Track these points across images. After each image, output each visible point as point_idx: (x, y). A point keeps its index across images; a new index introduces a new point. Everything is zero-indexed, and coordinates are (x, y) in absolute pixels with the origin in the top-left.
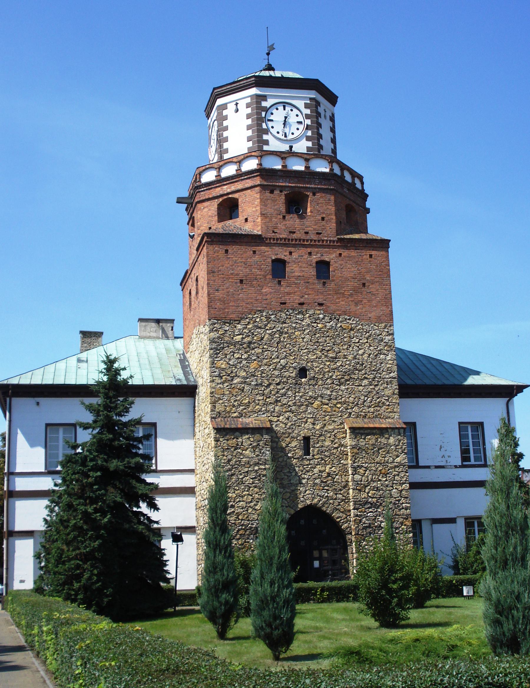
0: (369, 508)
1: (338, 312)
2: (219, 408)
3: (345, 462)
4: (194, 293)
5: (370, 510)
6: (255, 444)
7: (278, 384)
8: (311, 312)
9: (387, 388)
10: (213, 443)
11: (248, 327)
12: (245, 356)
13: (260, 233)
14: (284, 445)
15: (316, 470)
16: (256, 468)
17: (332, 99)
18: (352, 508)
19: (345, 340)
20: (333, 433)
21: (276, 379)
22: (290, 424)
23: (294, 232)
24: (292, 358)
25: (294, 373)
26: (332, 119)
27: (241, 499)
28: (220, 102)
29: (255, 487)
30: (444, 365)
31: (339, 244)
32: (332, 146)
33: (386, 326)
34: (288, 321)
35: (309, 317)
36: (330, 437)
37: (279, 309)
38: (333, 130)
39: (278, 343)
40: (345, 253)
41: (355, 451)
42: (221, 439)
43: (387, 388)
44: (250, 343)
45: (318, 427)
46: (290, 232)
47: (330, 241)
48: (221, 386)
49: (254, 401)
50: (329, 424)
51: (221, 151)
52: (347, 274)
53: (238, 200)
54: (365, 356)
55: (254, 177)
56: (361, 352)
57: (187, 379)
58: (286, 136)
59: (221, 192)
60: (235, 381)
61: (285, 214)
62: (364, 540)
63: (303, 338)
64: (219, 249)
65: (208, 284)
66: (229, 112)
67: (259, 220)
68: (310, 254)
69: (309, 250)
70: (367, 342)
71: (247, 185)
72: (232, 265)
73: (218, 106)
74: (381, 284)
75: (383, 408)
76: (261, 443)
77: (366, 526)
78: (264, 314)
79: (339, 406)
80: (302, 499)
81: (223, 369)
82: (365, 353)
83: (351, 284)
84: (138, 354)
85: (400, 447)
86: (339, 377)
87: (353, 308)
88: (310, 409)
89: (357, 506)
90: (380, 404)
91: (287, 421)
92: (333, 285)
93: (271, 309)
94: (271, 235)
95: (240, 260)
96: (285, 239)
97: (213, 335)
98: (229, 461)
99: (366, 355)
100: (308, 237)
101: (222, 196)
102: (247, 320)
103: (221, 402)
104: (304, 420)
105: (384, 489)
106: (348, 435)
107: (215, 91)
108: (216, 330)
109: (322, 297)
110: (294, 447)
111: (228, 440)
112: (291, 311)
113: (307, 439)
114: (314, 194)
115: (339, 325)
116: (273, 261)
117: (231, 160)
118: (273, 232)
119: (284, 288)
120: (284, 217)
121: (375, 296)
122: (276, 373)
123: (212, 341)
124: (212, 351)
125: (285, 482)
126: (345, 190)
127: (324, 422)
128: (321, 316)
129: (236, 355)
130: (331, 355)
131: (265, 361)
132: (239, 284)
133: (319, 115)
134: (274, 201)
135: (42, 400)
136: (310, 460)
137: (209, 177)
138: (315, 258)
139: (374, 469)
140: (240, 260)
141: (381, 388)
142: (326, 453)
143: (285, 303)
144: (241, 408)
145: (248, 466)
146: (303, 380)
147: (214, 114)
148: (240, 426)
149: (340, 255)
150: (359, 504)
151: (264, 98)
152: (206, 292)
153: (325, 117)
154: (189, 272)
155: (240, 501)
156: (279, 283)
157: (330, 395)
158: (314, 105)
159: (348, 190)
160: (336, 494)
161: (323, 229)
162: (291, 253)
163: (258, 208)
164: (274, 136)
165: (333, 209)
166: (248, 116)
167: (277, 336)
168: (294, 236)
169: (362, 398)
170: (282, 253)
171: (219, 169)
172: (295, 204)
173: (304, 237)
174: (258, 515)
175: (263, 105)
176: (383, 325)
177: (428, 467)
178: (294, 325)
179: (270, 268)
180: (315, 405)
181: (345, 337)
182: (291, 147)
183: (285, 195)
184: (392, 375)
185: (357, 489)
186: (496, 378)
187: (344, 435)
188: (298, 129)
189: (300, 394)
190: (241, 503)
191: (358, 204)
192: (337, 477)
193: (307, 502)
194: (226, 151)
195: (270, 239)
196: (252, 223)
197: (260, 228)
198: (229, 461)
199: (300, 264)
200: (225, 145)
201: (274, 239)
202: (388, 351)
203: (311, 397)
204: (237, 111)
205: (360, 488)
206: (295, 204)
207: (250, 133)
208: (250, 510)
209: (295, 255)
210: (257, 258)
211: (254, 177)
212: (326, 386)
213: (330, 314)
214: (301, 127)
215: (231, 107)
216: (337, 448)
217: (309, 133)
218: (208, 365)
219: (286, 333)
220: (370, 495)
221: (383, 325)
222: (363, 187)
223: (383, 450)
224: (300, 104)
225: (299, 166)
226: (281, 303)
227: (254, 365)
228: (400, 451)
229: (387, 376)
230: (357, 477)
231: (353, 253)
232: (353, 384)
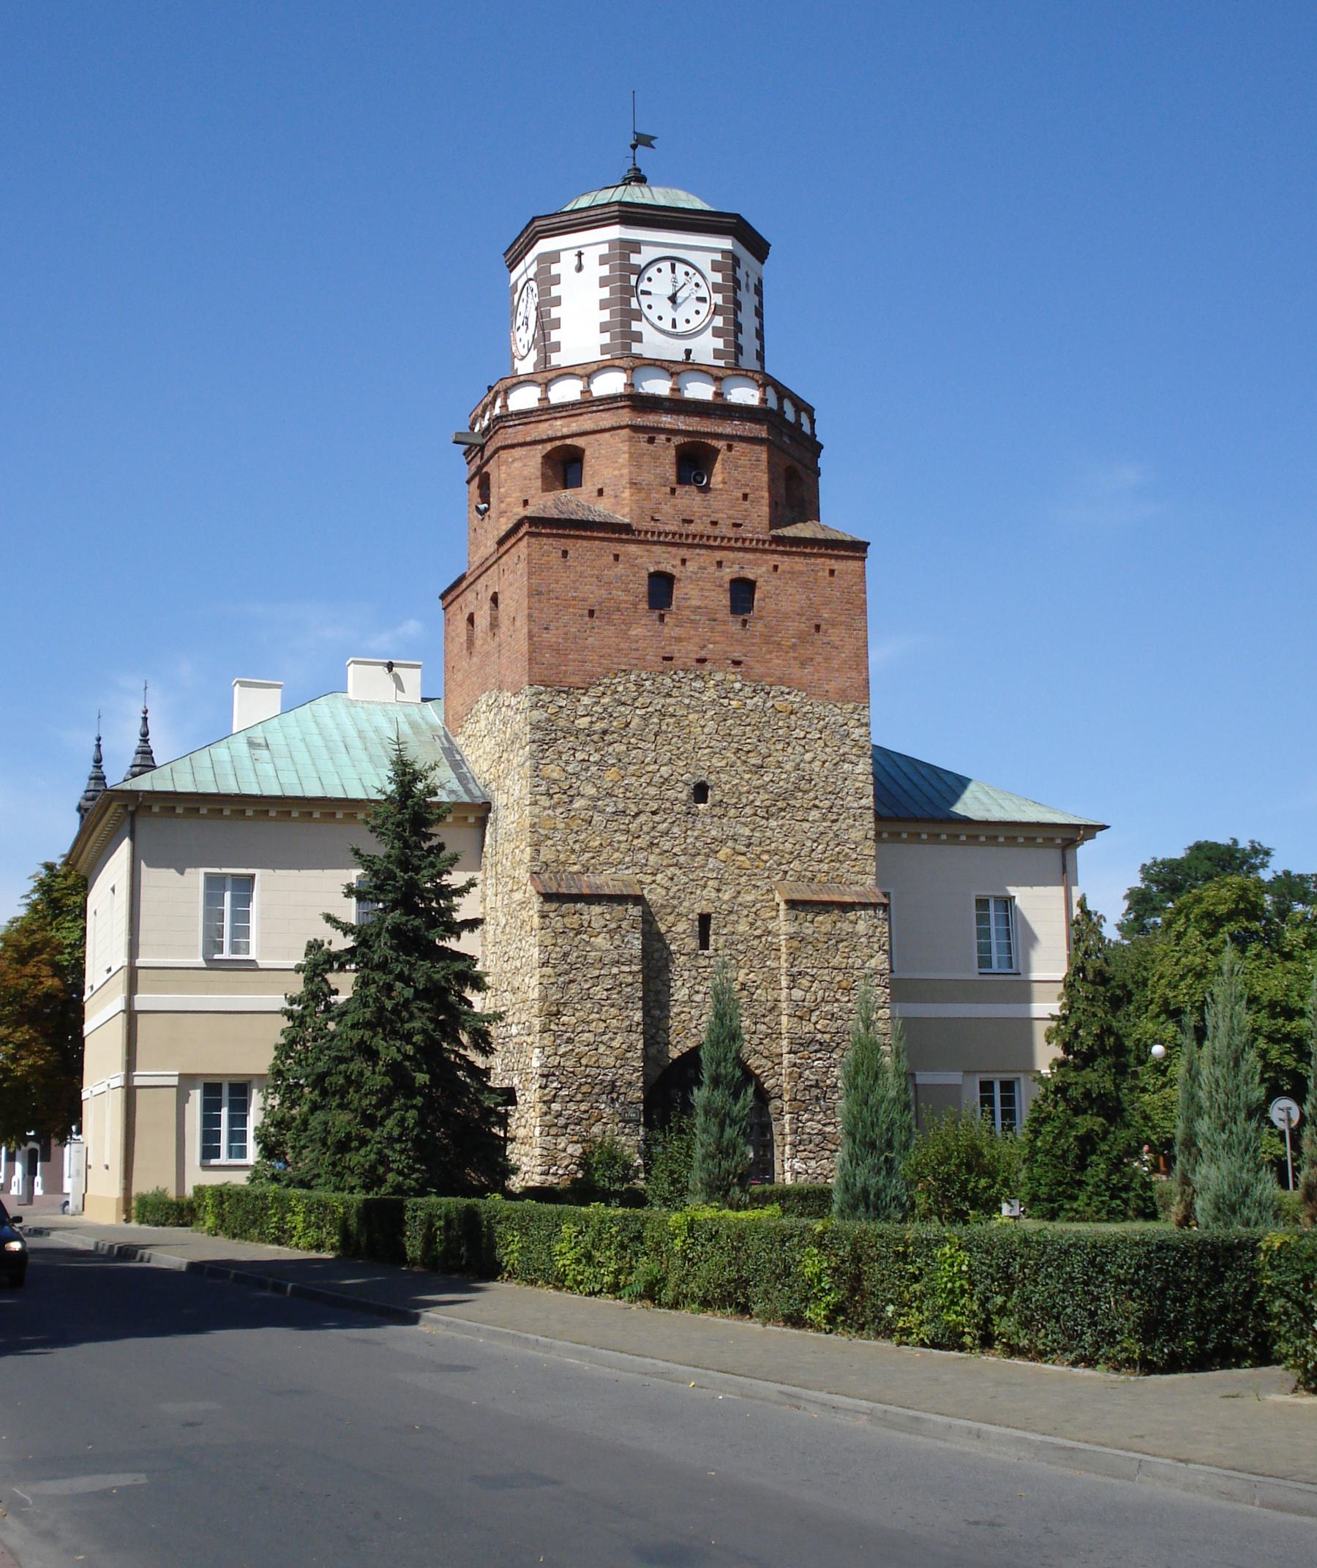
0: (816, 1051)
1: (768, 679)
2: (547, 854)
3: (774, 965)
4: (482, 621)
5: (819, 1055)
6: (613, 926)
7: (654, 813)
8: (719, 677)
9: (853, 826)
10: (536, 921)
13: (627, 520)
14: (663, 929)
16: (615, 970)
17: (759, 247)
18: (785, 1050)
19: (781, 732)
21: (651, 804)
22: (674, 889)
23: (691, 521)
24: (682, 764)
25: (685, 793)
26: (759, 291)
27: (586, 1028)
28: (544, 246)
29: (613, 1006)
30: (943, 776)
31: (773, 547)
33: (855, 708)
34: (675, 692)
37: (660, 669)
38: (759, 313)
39: (656, 735)
40: (786, 563)
41: (795, 944)
42: (551, 915)
43: (853, 826)
44: (605, 732)
45: (726, 897)
46: (685, 521)
47: (758, 541)
48: (550, 812)
49: (610, 844)
50: (748, 892)
51: (545, 346)
52: (786, 606)
53: (584, 451)
55: (618, 408)
56: (808, 756)
57: (468, 791)
58: (674, 326)
59: (551, 433)
60: (576, 805)
61: (675, 486)
62: (806, 1110)
63: (703, 727)
64: (550, 547)
65: (530, 616)
66: (564, 268)
67: (627, 494)
68: (720, 564)
69: (719, 555)
71: (607, 424)
72: (574, 582)
73: (540, 255)
74: (849, 627)
75: (845, 865)
76: (624, 924)
78: (633, 677)
79: (765, 857)
80: (694, 1031)
81: (555, 781)
82: (816, 760)
83: (795, 626)
84: (361, 734)
85: (875, 939)
86: (768, 803)
87: (796, 672)
88: (712, 863)
89: (795, 1048)
90: (841, 858)
91: (669, 884)
92: (759, 627)
93: (644, 668)
94: (649, 525)
95: (589, 572)
96: (674, 534)
97: (538, 715)
98: (566, 955)
99: (817, 763)
100: (717, 532)
101: (550, 440)
102: (601, 688)
103: (550, 842)
104: (702, 883)
105: (845, 1017)
106: (782, 913)
107: (537, 223)
108: (543, 706)
109: (738, 648)
110: (680, 933)
111: (563, 916)
112: (681, 674)
115: (769, 704)
116: (651, 576)
117: (571, 370)
118: (652, 519)
120: (673, 491)
121: (834, 649)
122: (652, 791)
123: (536, 727)
124: (534, 746)
127: (738, 888)
128: (737, 686)
129: (580, 756)
130: (753, 761)
131: (632, 768)
133: (737, 282)
134: (656, 458)
136: (710, 958)
137: (524, 399)
138: (729, 573)
139: (828, 978)
140: (589, 572)
141: (844, 826)
142: (740, 947)
143: (670, 659)
144: (588, 855)
145: (600, 966)
146: (701, 806)
147: (528, 266)
148: (586, 891)
149: (776, 568)
150: (798, 1044)
151: (635, 246)
152: (525, 630)
153: (747, 285)
154: (471, 579)
155: (582, 1032)
156: (662, 618)
157: (750, 838)
158: (730, 264)
159: (791, 438)
160: (756, 1023)
161: (745, 518)
162: (684, 561)
163: (625, 471)
164: (653, 325)
165: (765, 478)
166: (604, 282)
167: (656, 720)
168: (692, 528)
169: (809, 843)
170: (666, 560)
171: (546, 385)
172: (694, 463)
173: (709, 530)
174: (617, 1058)
175: (632, 261)
176: (851, 706)
178: (687, 701)
179: (645, 589)
180: (721, 855)
181: (780, 728)
182: (688, 352)
183: (678, 448)
184: (864, 802)
186: (1044, 809)
187: (774, 913)
188: (697, 312)
189: (696, 834)
190: (586, 1035)
191: (805, 466)
192: (759, 991)
194: (557, 347)
195: (646, 532)
196: (612, 500)
197: (627, 510)
198: (566, 955)
199: (700, 585)
200: (555, 336)
201: (653, 533)
202: (859, 756)
204: (579, 268)
205: (801, 1015)
206: (694, 463)
207: (605, 315)
208: (602, 1049)
209: (691, 566)
210: (620, 569)
211: (618, 408)
212: (743, 820)
213: (754, 681)
214: (704, 308)
215: (569, 260)
216: (759, 937)
217: (719, 321)
218: (527, 770)
219: (673, 716)
220: (818, 1026)
221: (851, 706)
222: (813, 428)
223: (845, 943)
224: (704, 261)
225: (700, 390)
226: (664, 658)
227: (611, 775)
228: (876, 947)
229: (855, 805)
230: (797, 994)
231: (799, 564)
232: (792, 818)
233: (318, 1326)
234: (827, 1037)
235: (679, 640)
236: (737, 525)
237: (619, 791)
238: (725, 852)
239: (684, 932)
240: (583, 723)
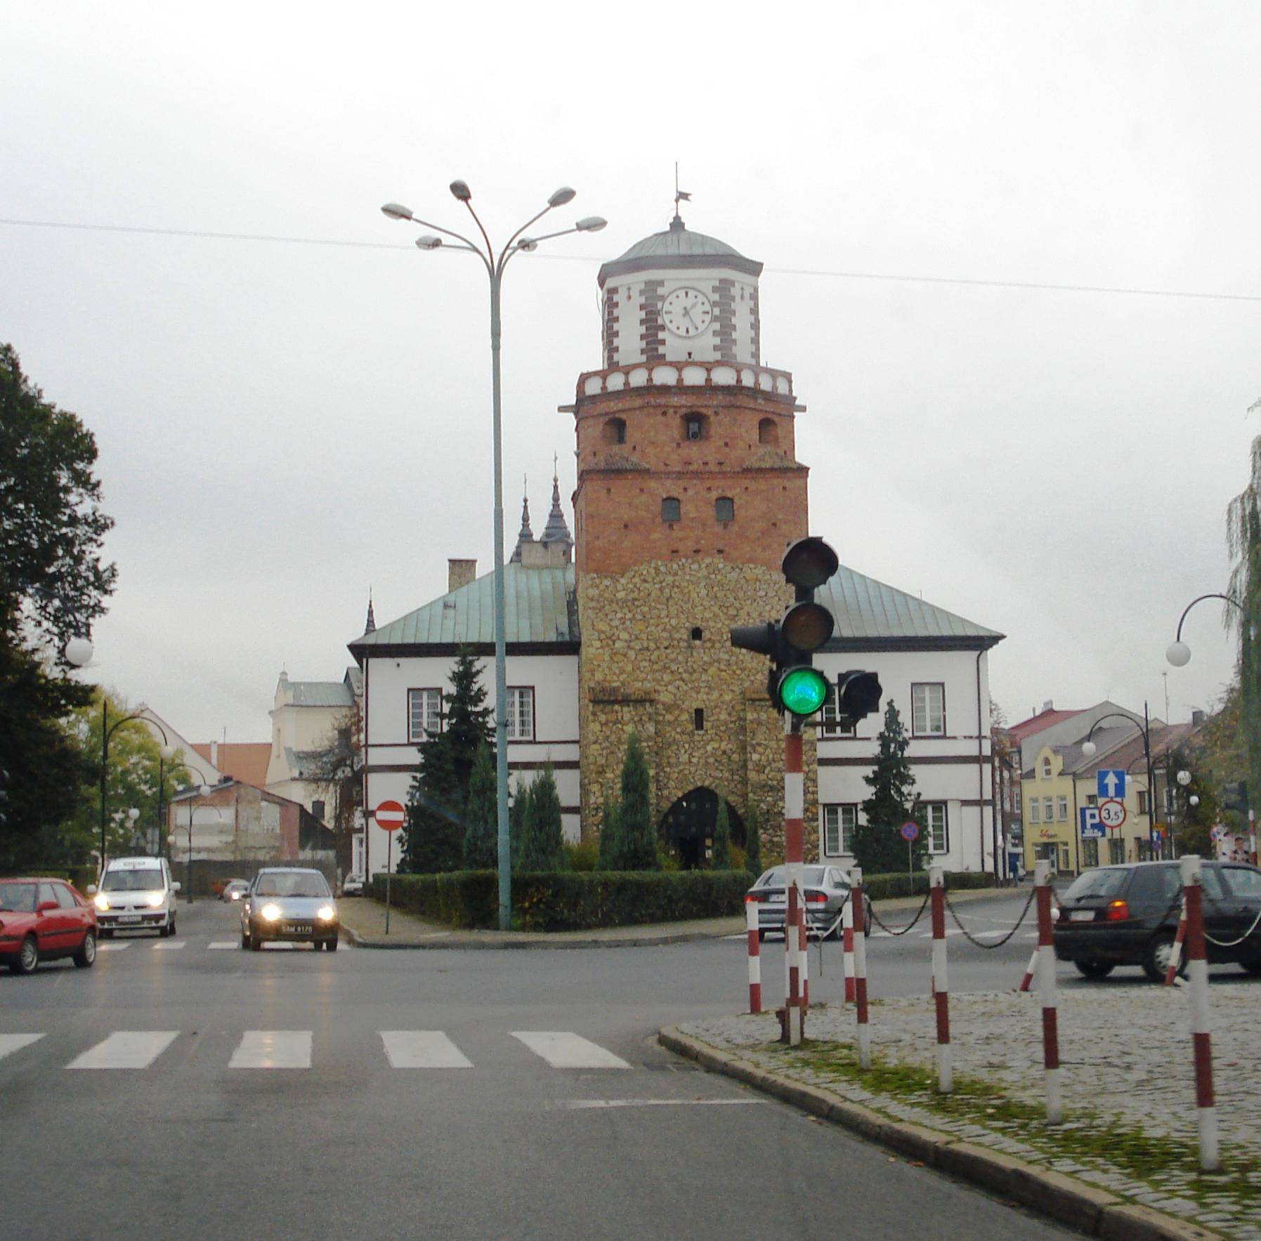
8: (708, 560)
12: (629, 616)
15: (709, 748)
32: (753, 333)
40: (752, 485)
44: (634, 599)
56: (768, 608)
94: (662, 468)
100: (707, 469)
101: (607, 414)
113: (699, 712)
114: (716, 413)
116: (664, 500)
119: (677, 532)
125: (673, 760)
126: (760, 401)
129: (619, 615)
135: (401, 660)
138: (715, 494)
144: (625, 676)
156: (671, 526)
162: (685, 489)
168: (691, 468)
177: (954, 738)
203: (705, 663)
204: (629, 298)
209: (690, 492)
210: (643, 498)
214: (708, 318)
233: (525, 1045)
236: (720, 464)
237: (644, 636)
238: (712, 670)
240: (621, 595)
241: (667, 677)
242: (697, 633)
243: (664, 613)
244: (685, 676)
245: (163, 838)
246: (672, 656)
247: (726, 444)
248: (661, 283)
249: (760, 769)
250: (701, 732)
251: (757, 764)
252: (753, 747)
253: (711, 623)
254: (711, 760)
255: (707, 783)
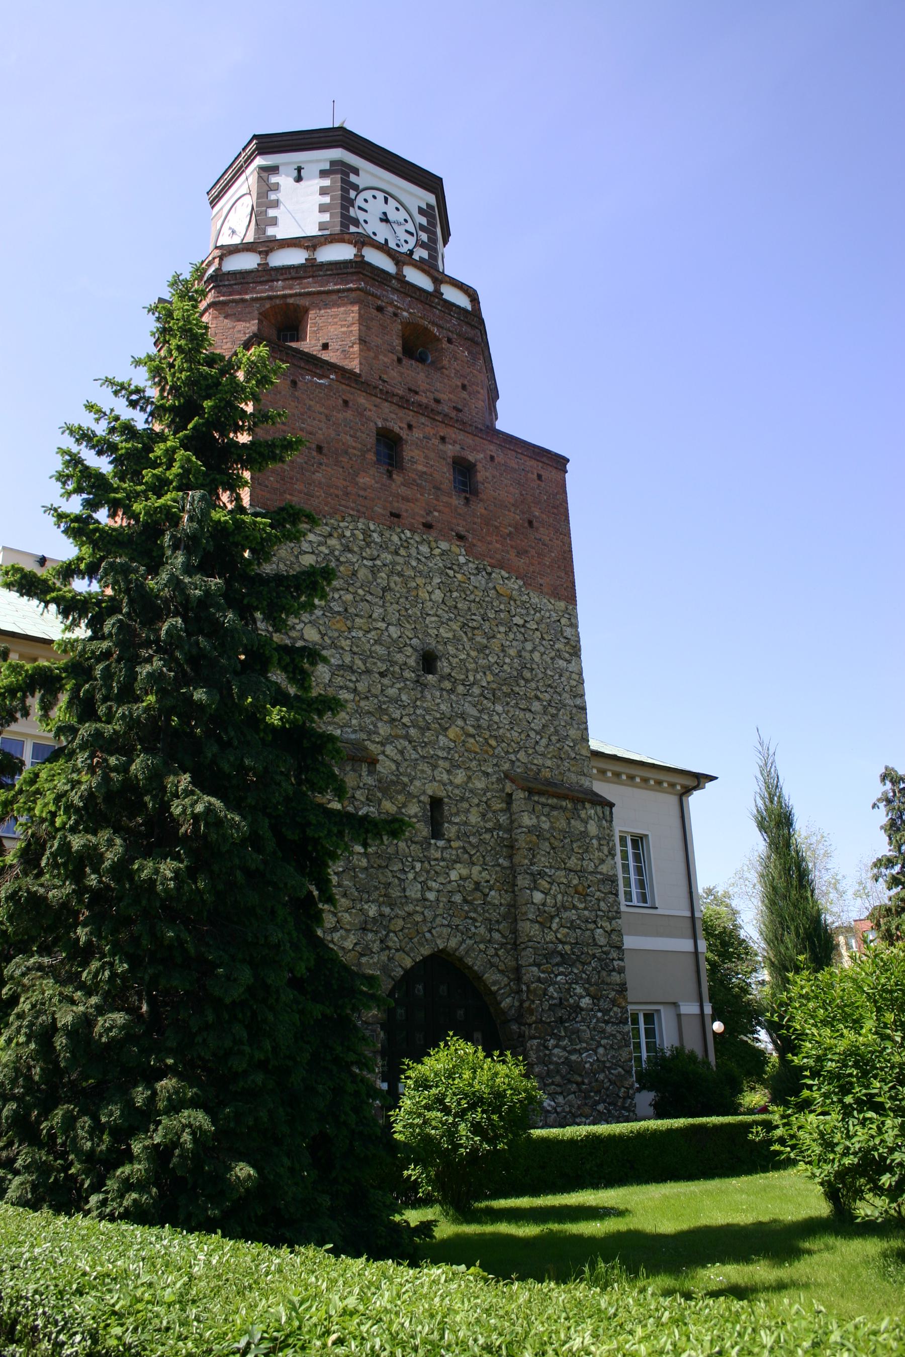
0: (557, 964)
5: (561, 969)
11: (329, 542)
15: (454, 875)
20: (484, 799)
21: (379, 664)
25: (413, 658)
35: (441, 555)
36: (478, 805)
54: (536, 656)
61: (401, 356)
67: (356, 348)
70: (537, 629)
77: (555, 1005)
105: (583, 926)
113: (436, 803)
125: (395, 893)
132: (314, 453)
134: (384, 327)
138: (451, 450)
142: (473, 840)
156: (390, 475)
157: (478, 719)
163: (355, 328)
171: (266, 253)
180: (451, 733)
185: (537, 922)
192: (493, 893)
193: (439, 942)
209: (417, 434)
234: (568, 947)
235: (406, 499)
239: (416, 816)
241: (384, 730)
242: (429, 661)
243: (378, 612)
244: (412, 731)
245: (579, 1037)
246: (392, 692)
247: (464, 387)
248: (356, 172)
249: (544, 920)
250: (441, 843)
251: (541, 909)
252: (535, 877)
253: (451, 649)
254: (458, 898)
255: (453, 943)
